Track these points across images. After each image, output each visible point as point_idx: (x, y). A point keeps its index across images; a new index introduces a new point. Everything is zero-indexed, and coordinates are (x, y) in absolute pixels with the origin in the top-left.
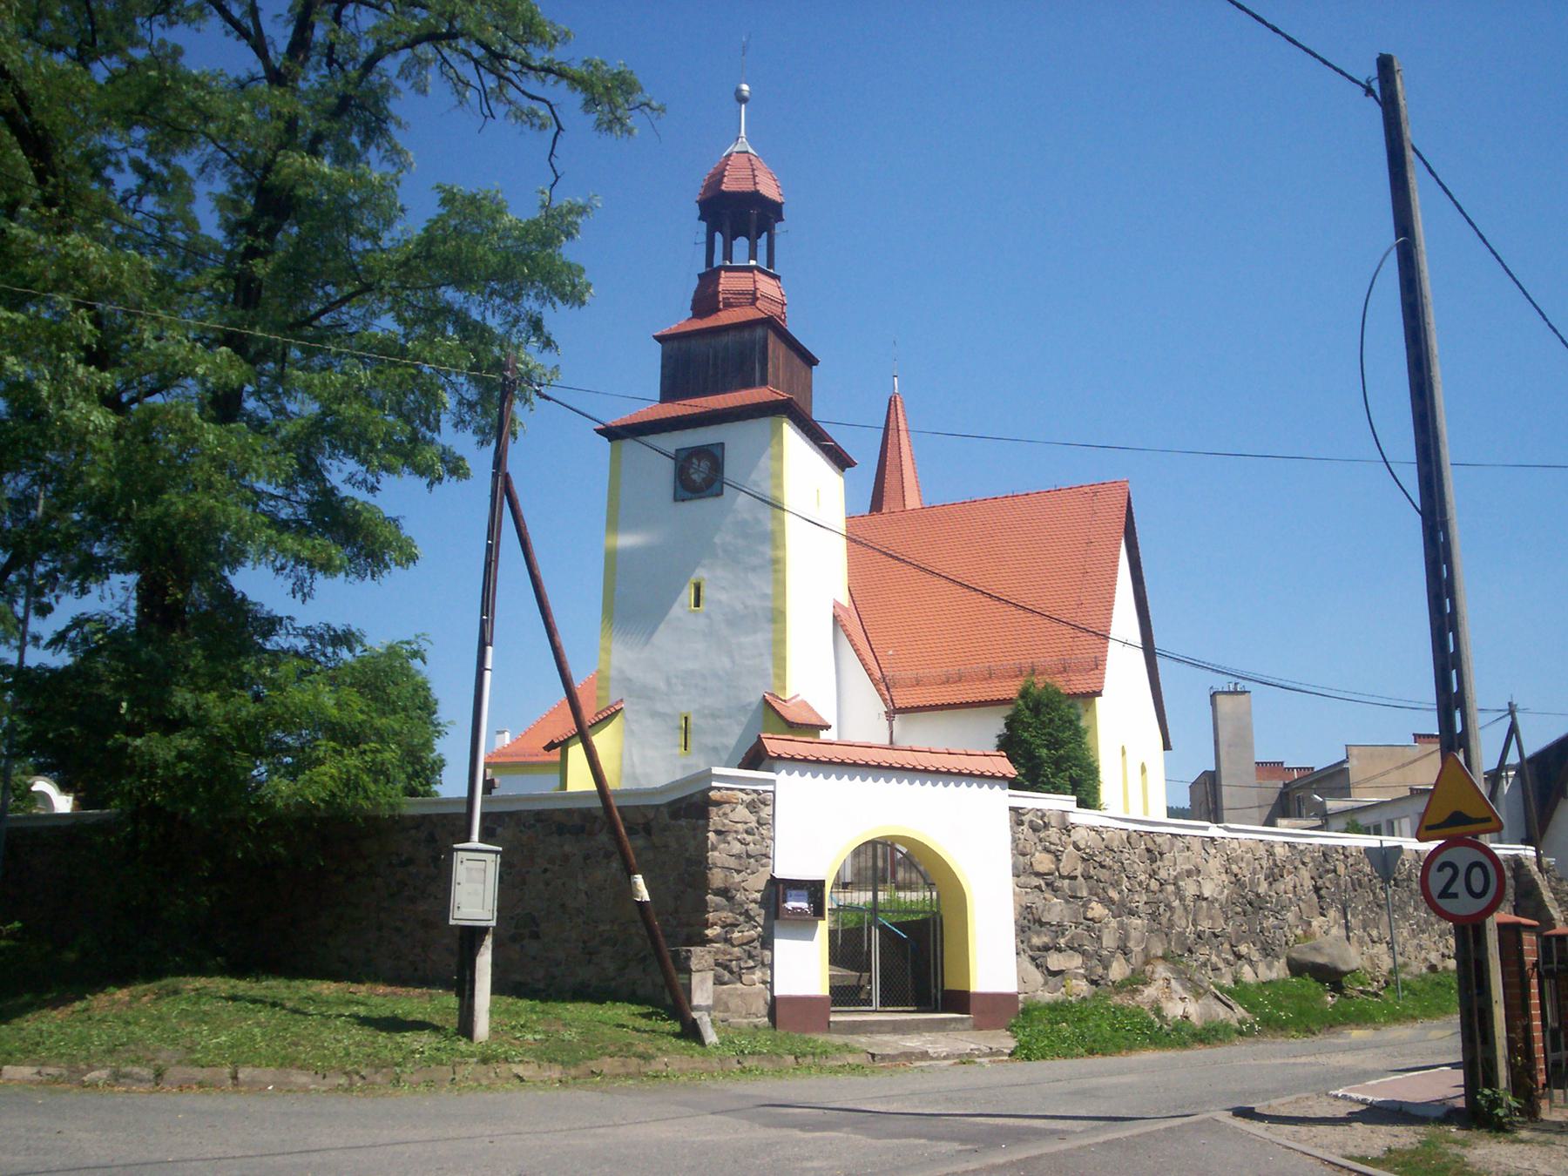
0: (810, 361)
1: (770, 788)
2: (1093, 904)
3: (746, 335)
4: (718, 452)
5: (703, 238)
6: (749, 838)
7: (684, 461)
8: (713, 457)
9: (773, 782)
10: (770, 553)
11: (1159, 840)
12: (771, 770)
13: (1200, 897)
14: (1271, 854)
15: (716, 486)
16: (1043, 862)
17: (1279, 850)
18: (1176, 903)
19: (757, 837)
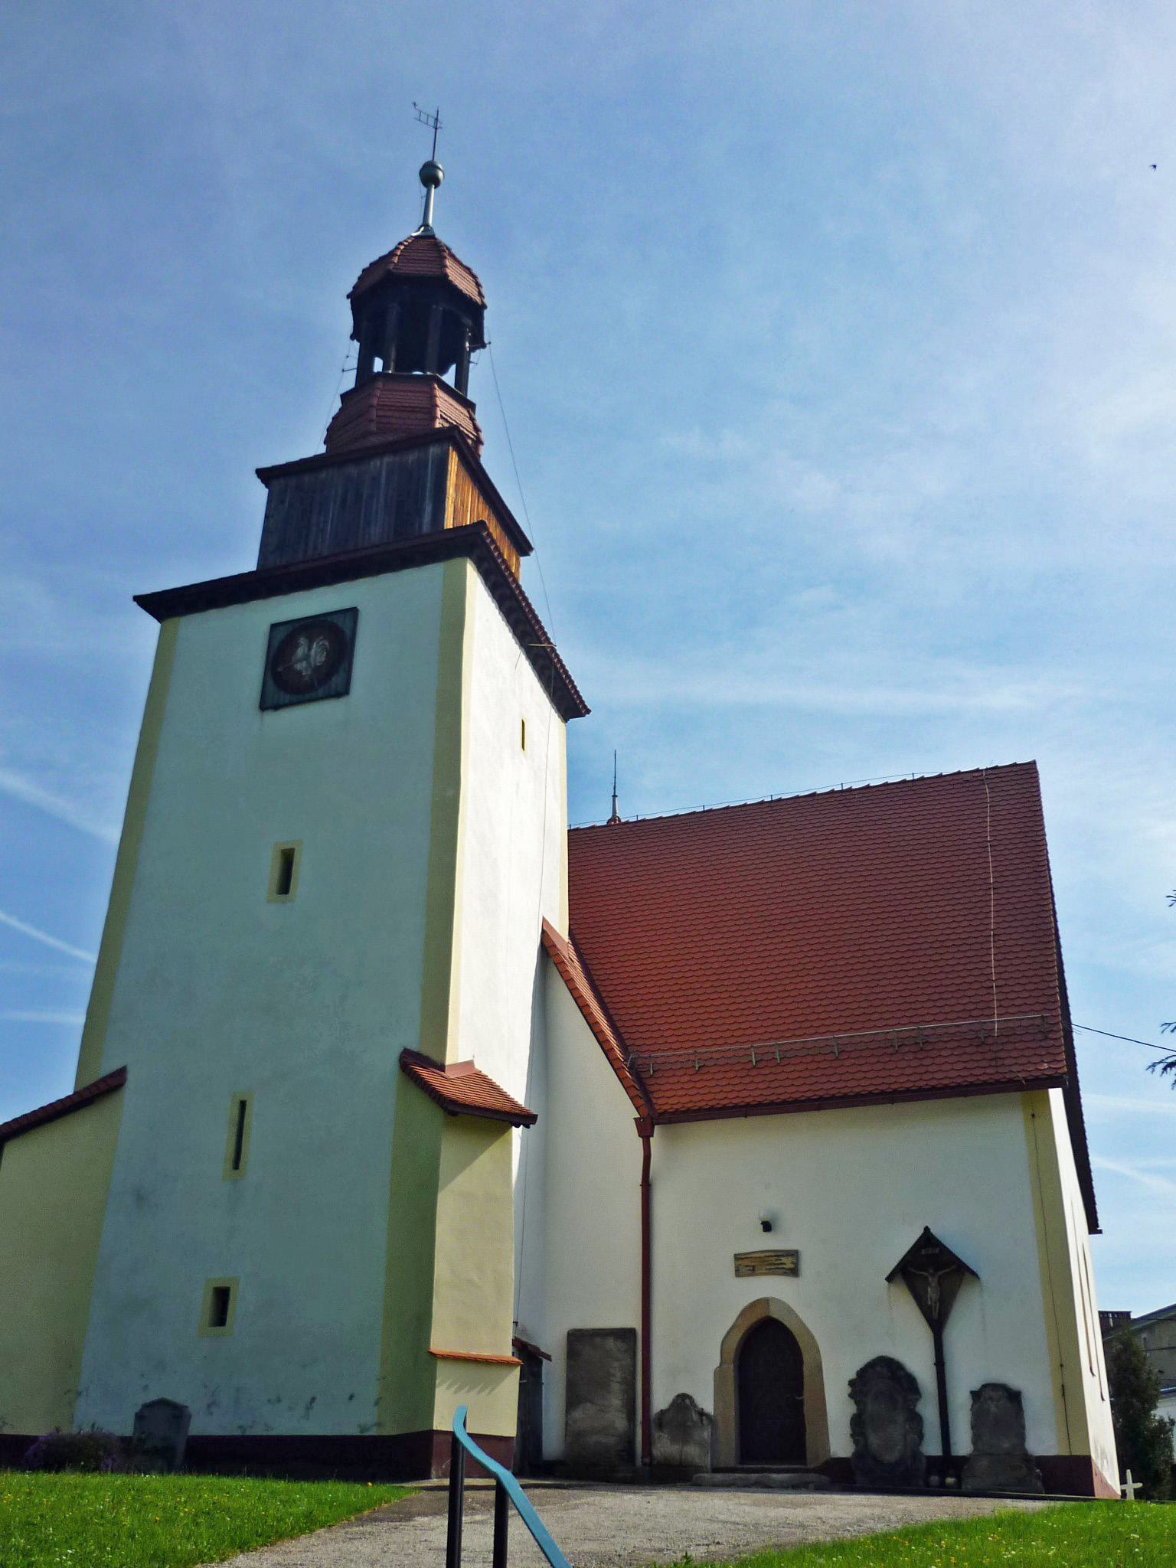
3: (412, 457)
4: (345, 624)
8: (337, 633)
15: (336, 681)
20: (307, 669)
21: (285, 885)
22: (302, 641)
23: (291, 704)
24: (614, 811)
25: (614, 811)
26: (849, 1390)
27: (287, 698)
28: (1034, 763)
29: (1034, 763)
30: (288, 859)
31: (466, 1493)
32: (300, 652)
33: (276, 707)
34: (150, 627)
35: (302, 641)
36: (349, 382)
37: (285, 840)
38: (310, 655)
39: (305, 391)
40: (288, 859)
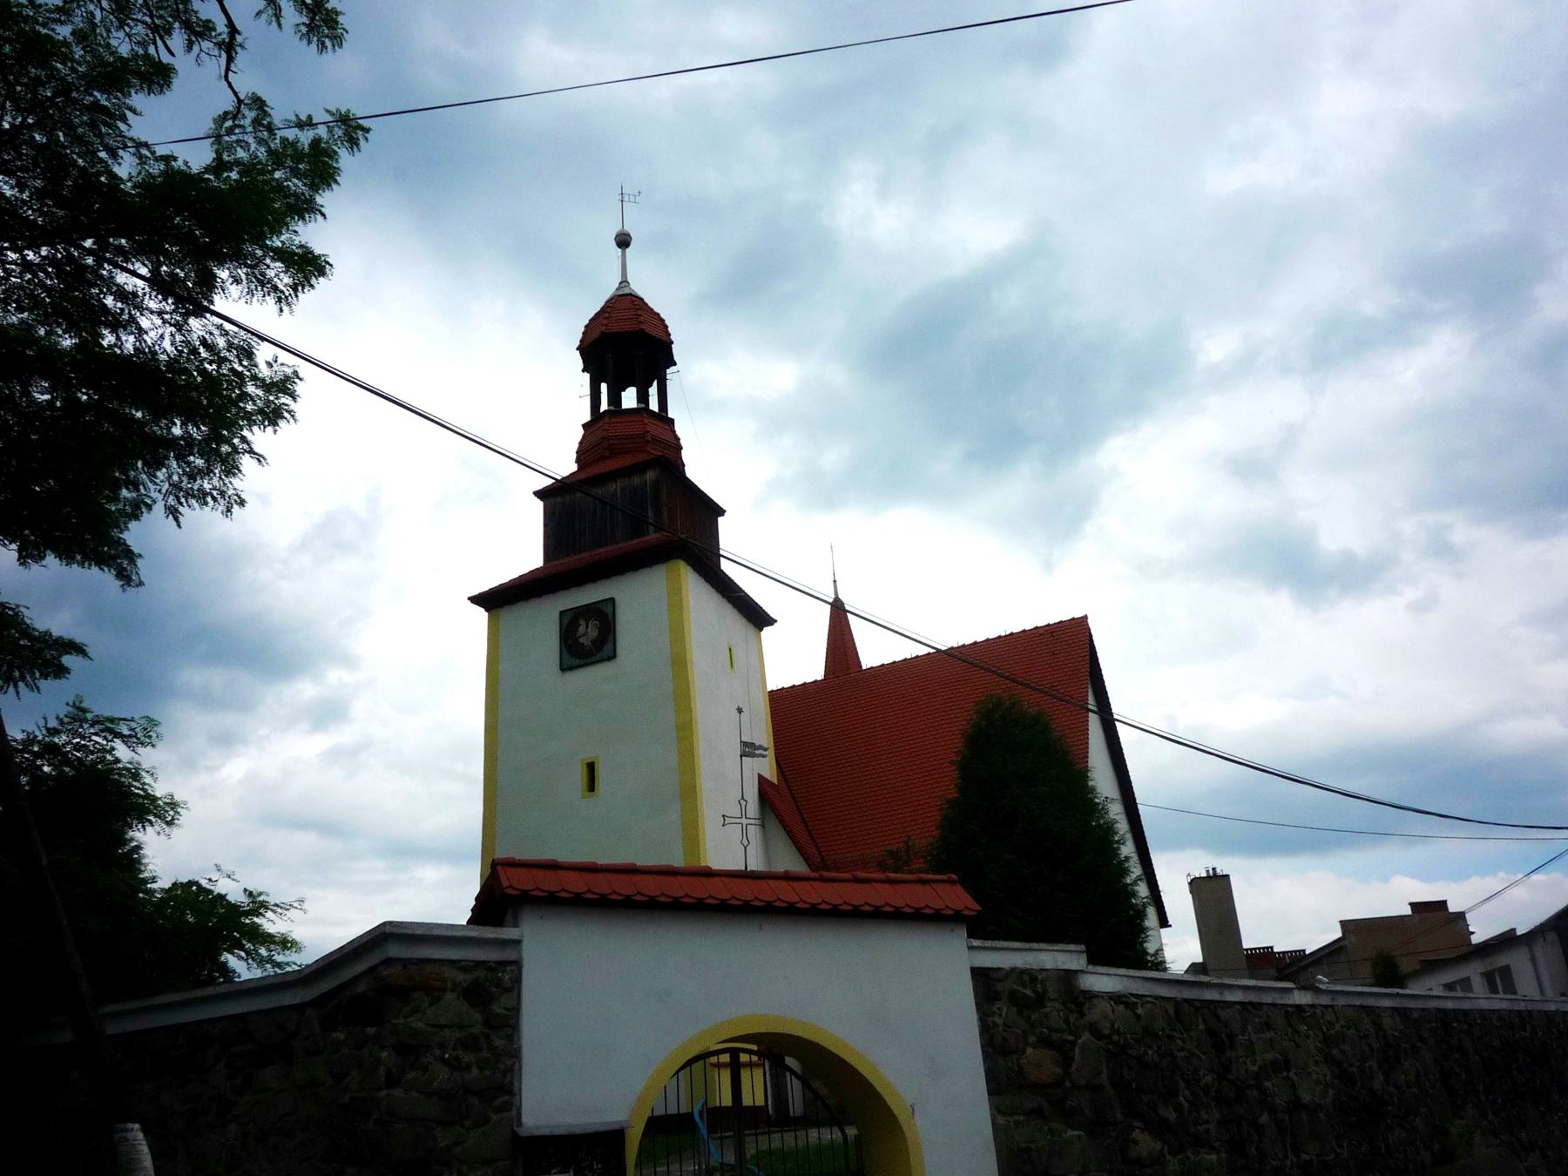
0: (758, 618)
1: (508, 955)
2: (1137, 1135)
3: (636, 480)
4: (608, 610)
5: (587, 390)
6: (467, 1057)
7: (570, 624)
8: (603, 617)
9: (517, 943)
10: (1001, 1120)
11: (1224, 1014)
12: (516, 925)
13: (1295, 1105)
14: (1378, 1026)
15: (608, 648)
16: (1039, 1062)
17: (1387, 1021)
18: (1264, 1119)
19: (485, 1054)
20: (589, 640)
21: (592, 786)
22: (582, 622)
23: (581, 666)
24: (235, 94)
25: (235, 94)
26: (233, 891)
27: (577, 662)
28: (1086, 617)
29: (1086, 617)
30: (591, 767)
31: (747, 1101)
32: (582, 629)
33: (571, 668)
34: (481, 615)
35: (582, 622)
36: (587, 417)
37: (588, 756)
38: (588, 632)
39: (554, 417)
40: (591, 767)
